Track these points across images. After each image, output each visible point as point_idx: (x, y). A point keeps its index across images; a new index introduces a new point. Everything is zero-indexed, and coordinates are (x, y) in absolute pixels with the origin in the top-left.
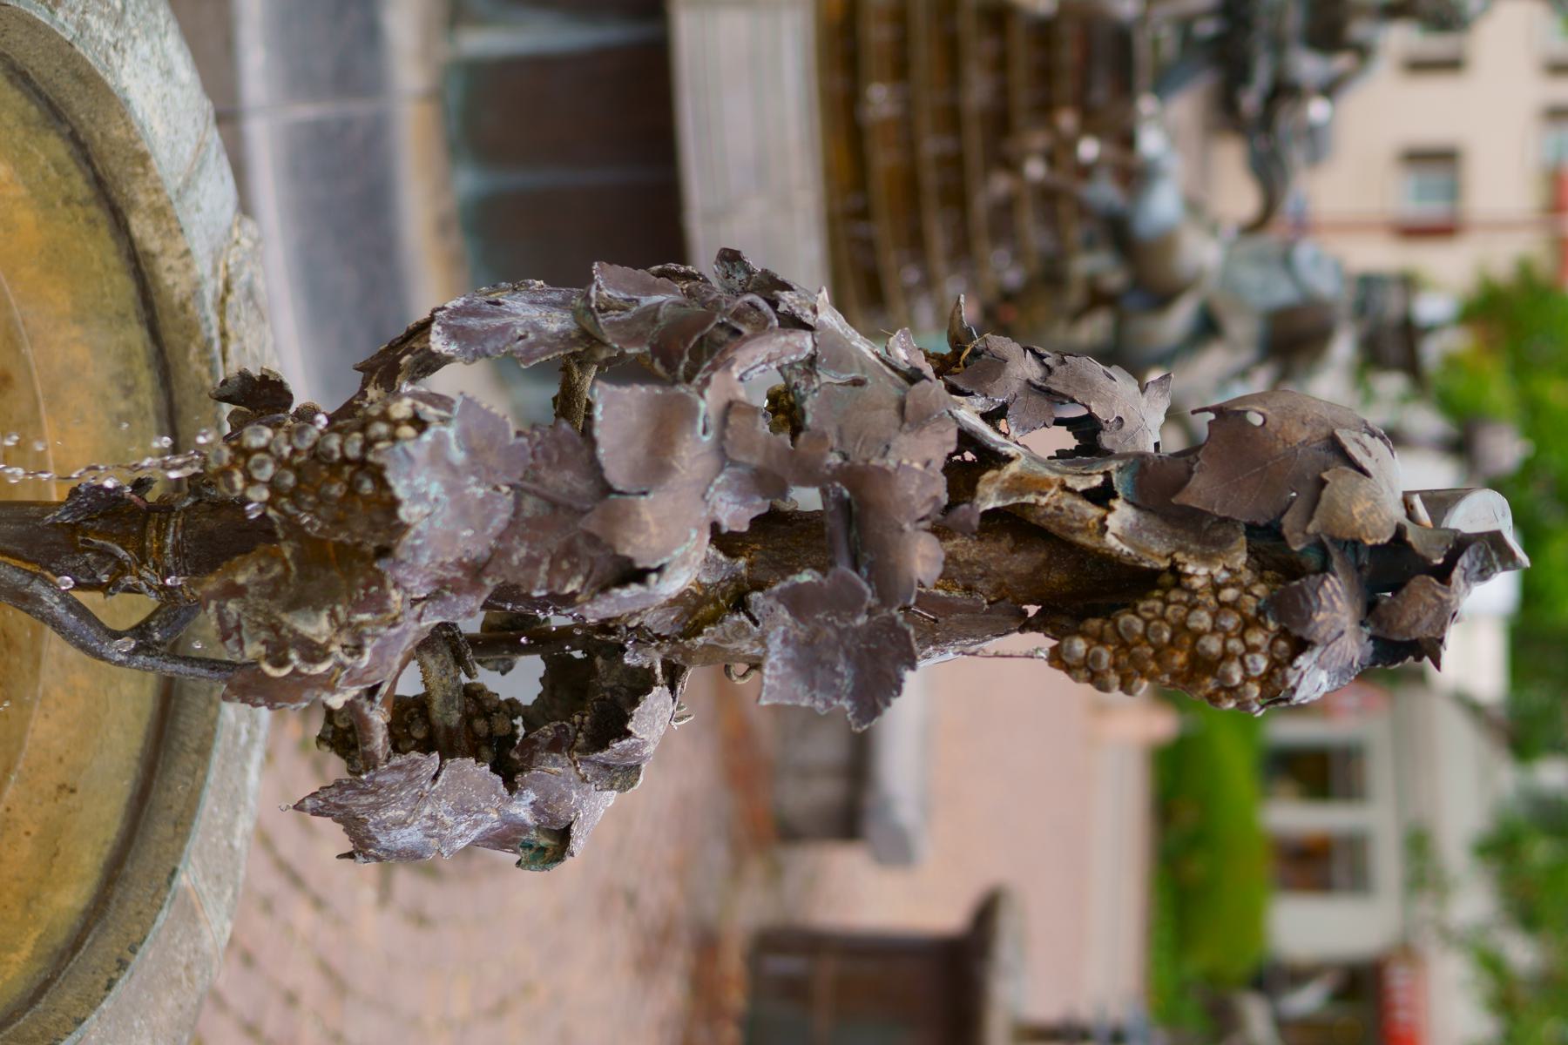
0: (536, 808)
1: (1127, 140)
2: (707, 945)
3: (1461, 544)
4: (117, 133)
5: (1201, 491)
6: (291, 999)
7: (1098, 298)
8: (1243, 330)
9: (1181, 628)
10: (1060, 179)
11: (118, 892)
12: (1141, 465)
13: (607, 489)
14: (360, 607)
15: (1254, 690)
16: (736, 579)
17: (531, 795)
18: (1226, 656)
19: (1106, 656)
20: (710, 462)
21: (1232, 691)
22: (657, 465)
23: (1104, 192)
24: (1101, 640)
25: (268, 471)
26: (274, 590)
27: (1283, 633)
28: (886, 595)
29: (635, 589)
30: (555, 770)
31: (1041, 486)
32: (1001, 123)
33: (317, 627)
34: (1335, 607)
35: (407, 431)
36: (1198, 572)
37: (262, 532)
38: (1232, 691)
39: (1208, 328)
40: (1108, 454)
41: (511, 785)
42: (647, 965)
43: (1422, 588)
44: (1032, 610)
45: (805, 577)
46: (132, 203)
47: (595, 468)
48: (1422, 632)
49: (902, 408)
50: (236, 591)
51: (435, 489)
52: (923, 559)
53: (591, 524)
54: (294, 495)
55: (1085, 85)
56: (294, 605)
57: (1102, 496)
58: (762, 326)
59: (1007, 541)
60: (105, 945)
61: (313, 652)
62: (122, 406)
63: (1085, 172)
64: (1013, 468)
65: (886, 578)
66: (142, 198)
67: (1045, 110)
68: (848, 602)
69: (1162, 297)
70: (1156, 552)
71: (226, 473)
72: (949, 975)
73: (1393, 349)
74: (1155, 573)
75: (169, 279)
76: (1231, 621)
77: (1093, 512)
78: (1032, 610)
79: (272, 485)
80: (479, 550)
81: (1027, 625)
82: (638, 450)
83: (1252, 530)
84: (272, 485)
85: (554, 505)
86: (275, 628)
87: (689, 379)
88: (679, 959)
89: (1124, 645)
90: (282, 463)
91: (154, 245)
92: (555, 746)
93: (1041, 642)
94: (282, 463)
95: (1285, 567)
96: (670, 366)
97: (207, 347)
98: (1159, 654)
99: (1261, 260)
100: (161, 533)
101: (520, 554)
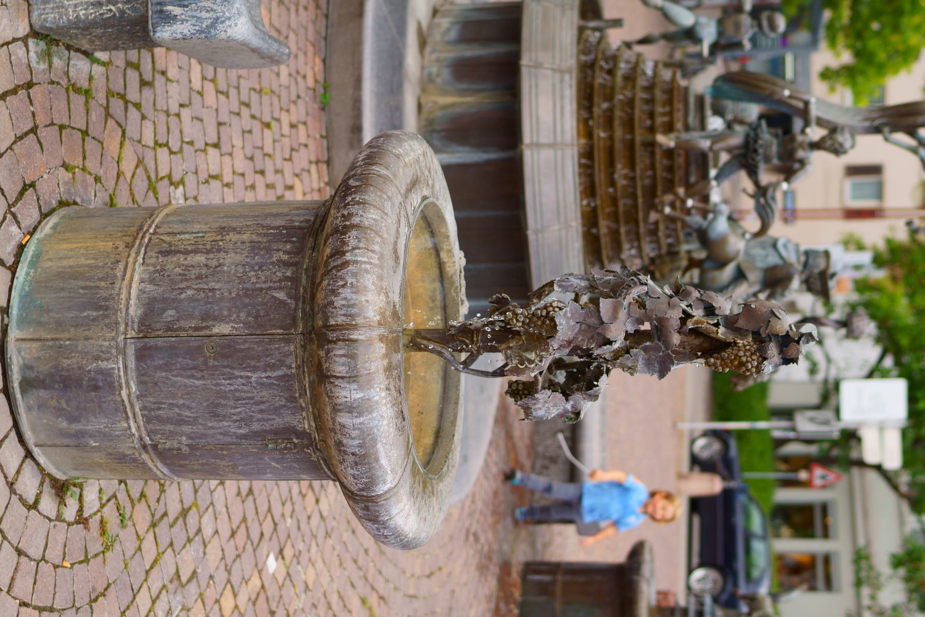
0: (573, 407)
1: (705, 199)
2: (505, 568)
3: (802, 335)
4: (443, 230)
5: (741, 323)
6: (366, 551)
7: (693, 263)
8: (754, 276)
9: (736, 355)
10: (677, 214)
11: (440, 440)
12: (726, 318)
13: (602, 323)
14: (543, 351)
15: (754, 370)
16: (626, 346)
17: (572, 402)
18: (747, 362)
19: (719, 362)
20: (626, 316)
21: (748, 370)
22: (614, 317)
23: (696, 219)
24: (717, 359)
25: (522, 319)
26: (520, 347)
27: (761, 356)
28: (667, 348)
29: (608, 346)
30: (578, 396)
31: (702, 323)
32: (651, 192)
33: (532, 356)
34: (773, 350)
35: (557, 309)
36: (740, 342)
37: (518, 333)
38: (748, 370)
39: (740, 276)
40: (717, 315)
41: (567, 400)
42: (482, 569)
43: (793, 346)
44: (699, 354)
45: (648, 344)
46: (442, 249)
47: (600, 318)
48: (793, 356)
49: (669, 304)
50: (510, 348)
51: (564, 323)
52: (676, 339)
53: (599, 331)
54: (528, 324)
55: (687, 174)
56: (526, 350)
57: (717, 325)
58: (635, 284)
59: (693, 336)
60: (440, 453)
61: (531, 361)
62: (431, 305)
63: (688, 212)
64: (695, 318)
65: (667, 344)
66: (445, 247)
67: (670, 187)
68: (657, 349)
69: (722, 264)
70: (730, 338)
71: (512, 319)
72: (622, 578)
73: (818, 285)
74: (730, 343)
75: (448, 269)
76: (748, 354)
77: (715, 329)
78: (699, 354)
79: (523, 322)
80: (571, 338)
81: (698, 357)
82: (610, 314)
83: (753, 333)
84: (523, 322)
85: (589, 326)
86: (521, 356)
87: (620, 295)
88: (495, 569)
89: (723, 360)
90: (526, 317)
91: (446, 260)
92: (577, 390)
93: (702, 361)
94: (526, 317)
95: (761, 341)
96: (615, 293)
97: (456, 289)
98: (732, 361)
99: (763, 247)
100: (477, 337)
101: (580, 338)
